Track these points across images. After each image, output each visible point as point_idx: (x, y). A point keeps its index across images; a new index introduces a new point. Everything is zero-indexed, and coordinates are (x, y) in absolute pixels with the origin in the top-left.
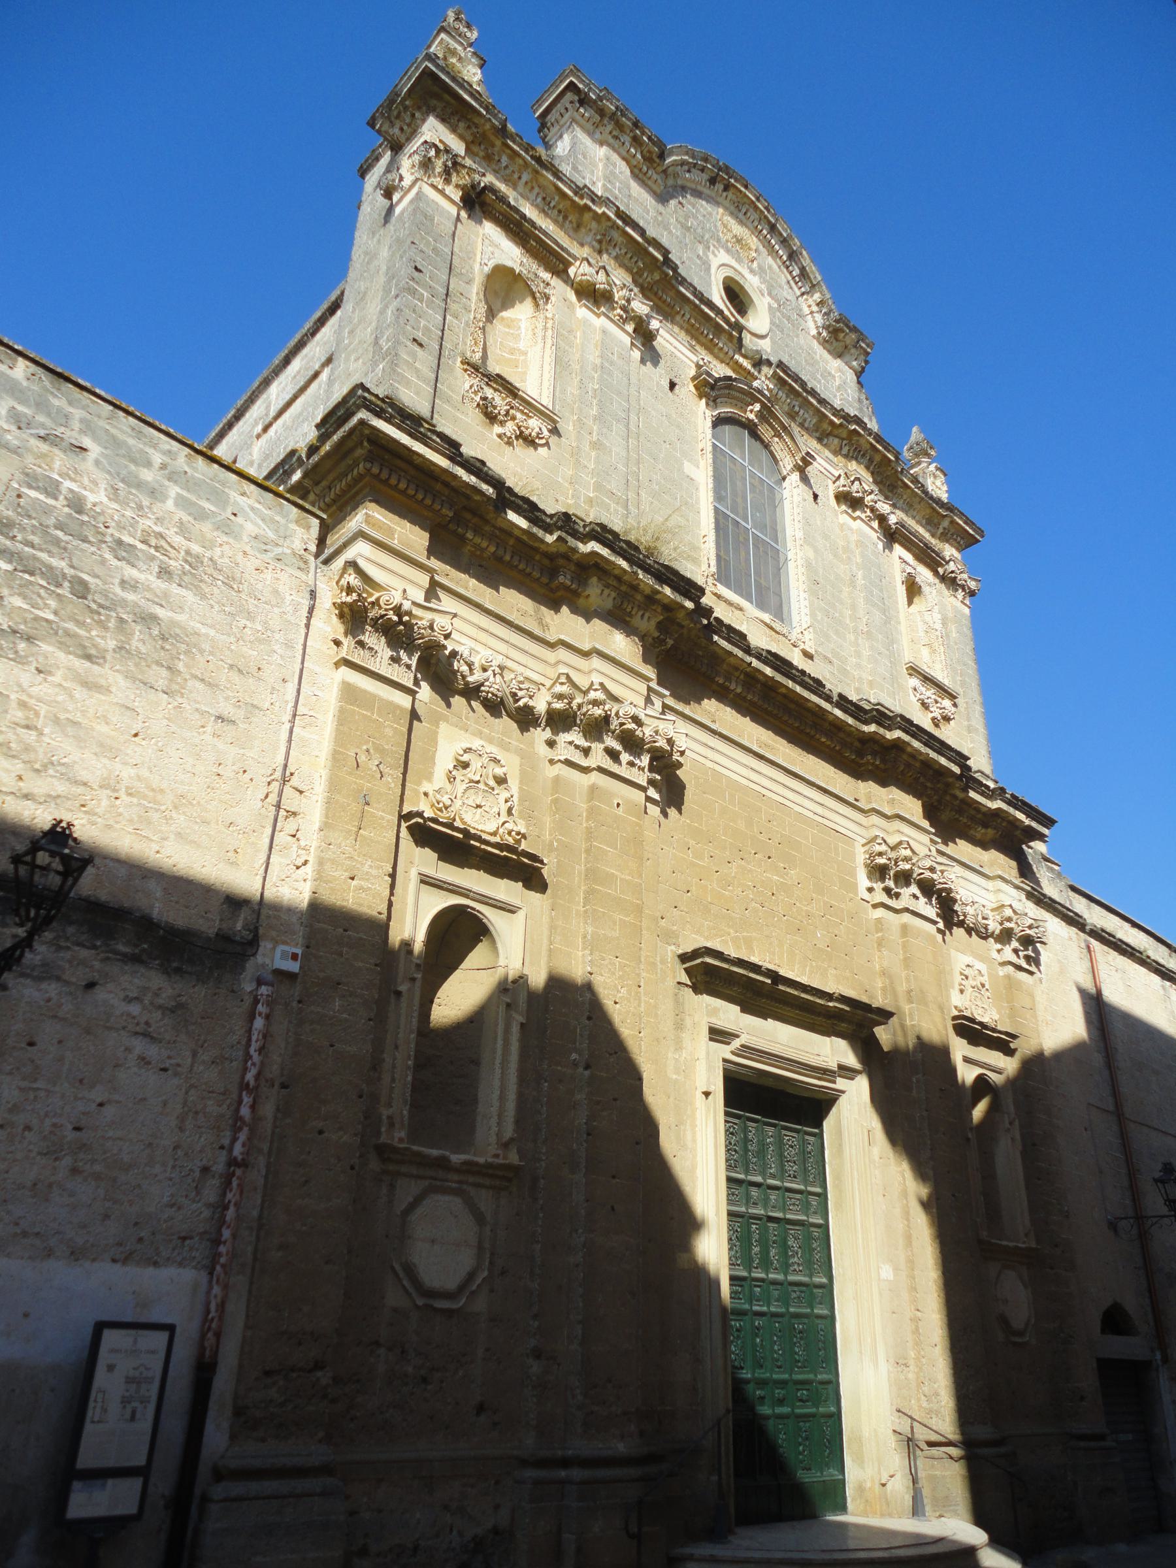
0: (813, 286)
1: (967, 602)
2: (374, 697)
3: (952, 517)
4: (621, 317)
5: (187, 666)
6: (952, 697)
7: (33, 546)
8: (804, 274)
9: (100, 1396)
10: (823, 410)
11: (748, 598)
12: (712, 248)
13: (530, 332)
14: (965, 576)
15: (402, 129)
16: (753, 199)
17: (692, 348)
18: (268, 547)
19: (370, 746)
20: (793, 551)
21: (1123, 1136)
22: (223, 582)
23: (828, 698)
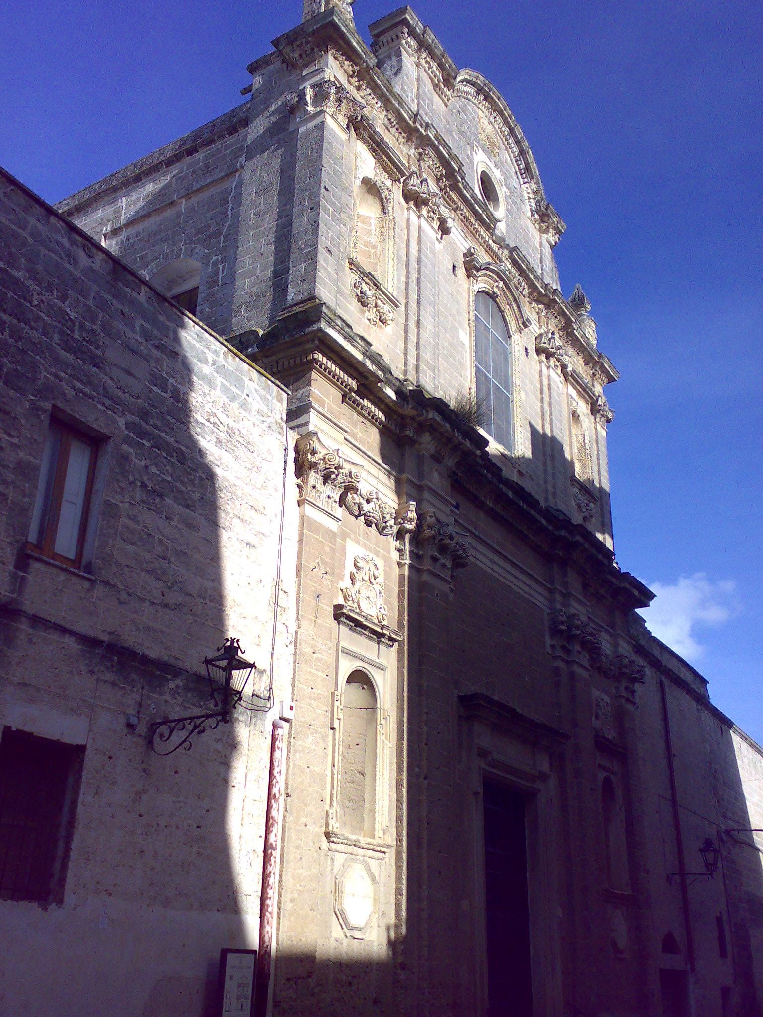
0: (532, 178)
2: (320, 526)
3: (602, 363)
5: (232, 509)
7: (158, 429)
8: (527, 168)
9: (228, 994)
10: (537, 283)
12: (475, 148)
13: (378, 231)
15: (300, 55)
16: (502, 108)
17: (466, 238)
18: (264, 419)
19: (319, 560)
21: (675, 815)
22: (245, 447)
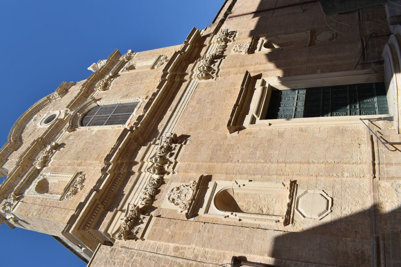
1: (134, 53)
6: (160, 56)
14: (127, 54)
23: (158, 92)
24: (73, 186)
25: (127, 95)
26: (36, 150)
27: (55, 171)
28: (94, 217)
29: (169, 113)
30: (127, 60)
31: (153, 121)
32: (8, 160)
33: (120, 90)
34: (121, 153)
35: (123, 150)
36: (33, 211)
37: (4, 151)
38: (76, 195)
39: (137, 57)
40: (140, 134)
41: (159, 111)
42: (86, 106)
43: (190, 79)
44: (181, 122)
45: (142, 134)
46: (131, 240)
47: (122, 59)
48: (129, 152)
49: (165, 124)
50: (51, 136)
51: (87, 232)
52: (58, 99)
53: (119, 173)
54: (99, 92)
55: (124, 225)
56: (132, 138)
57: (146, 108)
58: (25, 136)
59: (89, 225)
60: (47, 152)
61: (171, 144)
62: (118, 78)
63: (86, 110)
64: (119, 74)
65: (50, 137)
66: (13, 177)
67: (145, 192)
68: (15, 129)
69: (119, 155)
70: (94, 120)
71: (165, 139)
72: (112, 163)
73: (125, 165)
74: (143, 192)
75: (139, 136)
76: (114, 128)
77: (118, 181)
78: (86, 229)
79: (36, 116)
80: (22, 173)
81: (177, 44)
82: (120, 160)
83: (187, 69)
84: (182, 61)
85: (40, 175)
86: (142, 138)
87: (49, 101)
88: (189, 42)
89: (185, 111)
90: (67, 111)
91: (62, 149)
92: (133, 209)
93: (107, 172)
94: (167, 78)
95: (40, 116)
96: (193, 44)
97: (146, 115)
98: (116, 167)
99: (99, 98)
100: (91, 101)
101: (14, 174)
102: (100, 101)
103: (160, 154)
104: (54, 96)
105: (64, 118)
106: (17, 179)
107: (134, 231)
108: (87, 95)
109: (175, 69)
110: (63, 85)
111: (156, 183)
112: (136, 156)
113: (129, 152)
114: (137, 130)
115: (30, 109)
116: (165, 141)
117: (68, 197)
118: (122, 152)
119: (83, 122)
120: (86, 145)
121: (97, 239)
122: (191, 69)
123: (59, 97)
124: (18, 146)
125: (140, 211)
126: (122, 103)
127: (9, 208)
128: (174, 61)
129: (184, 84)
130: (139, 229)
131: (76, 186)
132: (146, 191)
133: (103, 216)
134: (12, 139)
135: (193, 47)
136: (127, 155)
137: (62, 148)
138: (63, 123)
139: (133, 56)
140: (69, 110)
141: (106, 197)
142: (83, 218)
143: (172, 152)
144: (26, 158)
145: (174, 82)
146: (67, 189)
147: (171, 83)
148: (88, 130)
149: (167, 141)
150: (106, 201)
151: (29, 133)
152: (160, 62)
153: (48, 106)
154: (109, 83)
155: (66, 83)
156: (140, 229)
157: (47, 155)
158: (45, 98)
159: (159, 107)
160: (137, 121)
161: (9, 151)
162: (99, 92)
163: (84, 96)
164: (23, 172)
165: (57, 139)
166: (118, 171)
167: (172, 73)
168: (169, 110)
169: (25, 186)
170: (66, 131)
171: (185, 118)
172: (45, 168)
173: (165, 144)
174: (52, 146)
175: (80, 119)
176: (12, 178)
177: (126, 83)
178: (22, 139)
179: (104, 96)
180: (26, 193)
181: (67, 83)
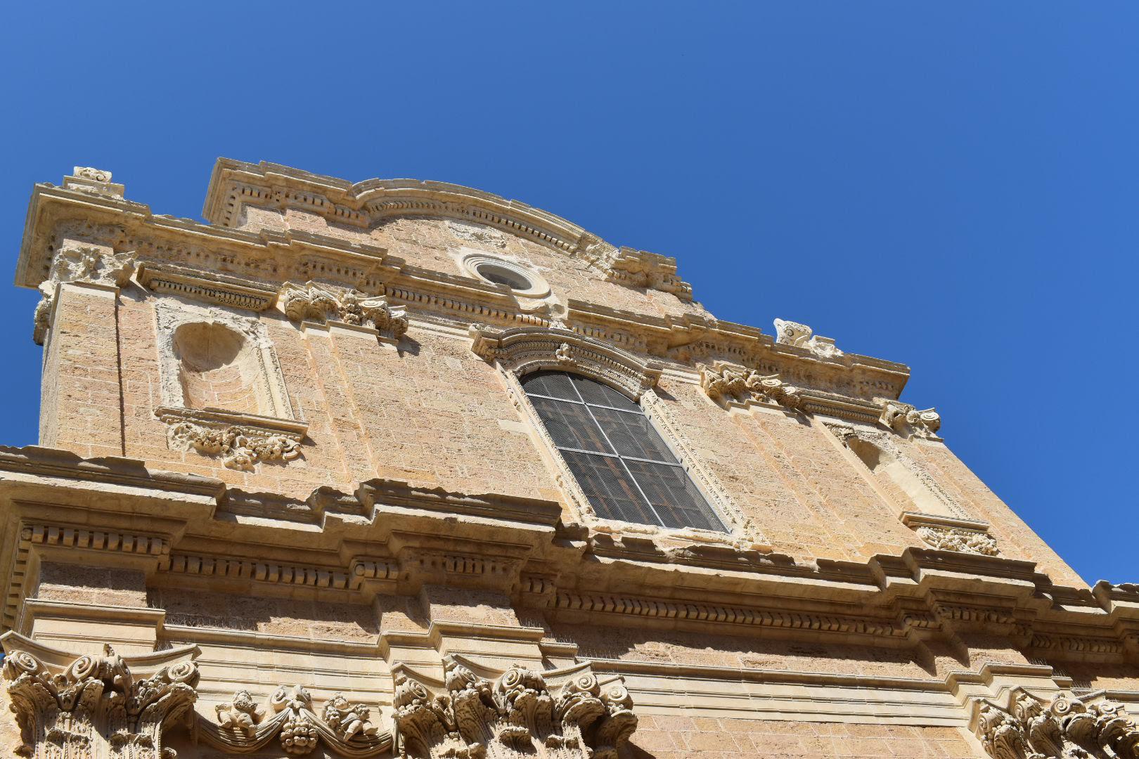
1: (933, 435)
4: (354, 320)
6: (982, 530)
11: (652, 520)
14: (912, 412)
20: (686, 460)
23: (806, 572)
24: (238, 434)
25: (737, 479)
26: (351, 273)
27: (286, 361)
28: (98, 543)
29: (736, 660)
30: (888, 426)
31: (663, 612)
32: (283, 213)
33: (746, 447)
34: (438, 538)
35: (458, 541)
36: (86, 343)
37: (309, 188)
38: (201, 457)
39: (926, 450)
40: (572, 584)
41: (722, 617)
42: (610, 360)
43: (949, 682)
44: (717, 727)
45: (576, 590)
46: (19, 731)
47: (882, 405)
48: (460, 568)
49: (673, 663)
50: (433, 300)
51: (23, 545)
52: (597, 272)
53: (347, 568)
54: (696, 382)
55: (80, 666)
56: (535, 553)
57: (704, 555)
58: (398, 230)
59: (53, 537)
60: (355, 302)
61: (573, 721)
62: (794, 421)
63: (595, 370)
64: (813, 418)
65: (425, 299)
66: (211, 241)
67: (289, 704)
68: (412, 192)
69: (426, 530)
70: (569, 413)
71: (585, 681)
72: (374, 517)
73: (394, 574)
74: (284, 695)
75: (557, 580)
76: (561, 485)
77: (311, 580)
78: (32, 534)
79: (498, 234)
80: (243, 265)
81: (1078, 571)
82: (405, 547)
83: (988, 648)
84: (1007, 612)
85: (254, 319)
86: (554, 600)
87: (572, 247)
88: (1116, 604)
89: (780, 724)
90: (559, 309)
91: (390, 348)
92: (171, 676)
93: (327, 514)
94: (890, 580)
95: (504, 246)
96: (1123, 626)
97: (670, 567)
98: (365, 544)
99: (669, 393)
100: (638, 369)
101: (224, 243)
102: (660, 399)
103: (502, 690)
104: (600, 254)
105: (528, 313)
106: (212, 257)
107: (62, 727)
108: (661, 348)
109: (953, 599)
110: (656, 262)
111: (350, 730)
112: (454, 604)
113: (460, 568)
114: (579, 559)
115: (512, 205)
116: (575, 690)
117: (180, 435)
118: (446, 539)
119: (541, 379)
120: (443, 419)
121: (15, 607)
122: (995, 663)
123: (605, 271)
124: (350, 220)
125: (176, 713)
126: (692, 474)
127: (79, 272)
128: (984, 579)
129: (912, 666)
130: (82, 743)
131: (238, 445)
132: (292, 706)
133: (121, 579)
134: (369, 195)
135: (1108, 634)
136: (444, 564)
137: (395, 349)
138: (506, 316)
139: (920, 437)
140: (565, 315)
141: (215, 560)
142: (75, 502)
143: (536, 742)
144: (303, 253)
145: (894, 623)
146: (213, 417)
147: (883, 613)
148: (512, 401)
149: (580, 694)
150: (194, 566)
151: (416, 237)
152: (956, 536)
153: (553, 253)
154: (753, 399)
155: (672, 269)
156: (82, 748)
157: (342, 309)
158: (578, 231)
159: (736, 609)
160: (622, 545)
161: (318, 201)
162: (696, 382)
163: (648, 342)
164: (248, 265)
165: (429, 322)
166: (353, 561)
167: (926, 595)
168: (751, 655)
169: (188, 290)
170: (472, 335)
171: (744, 740)
172: (287, 325)
173: (559, 696)
174: (387, 310)
175: (548, 362)
176: (204, 239)
177: (784, 454)
178: (383, 225)
179: (689, 405)
180: (161, 301)
181: (674, 273)
